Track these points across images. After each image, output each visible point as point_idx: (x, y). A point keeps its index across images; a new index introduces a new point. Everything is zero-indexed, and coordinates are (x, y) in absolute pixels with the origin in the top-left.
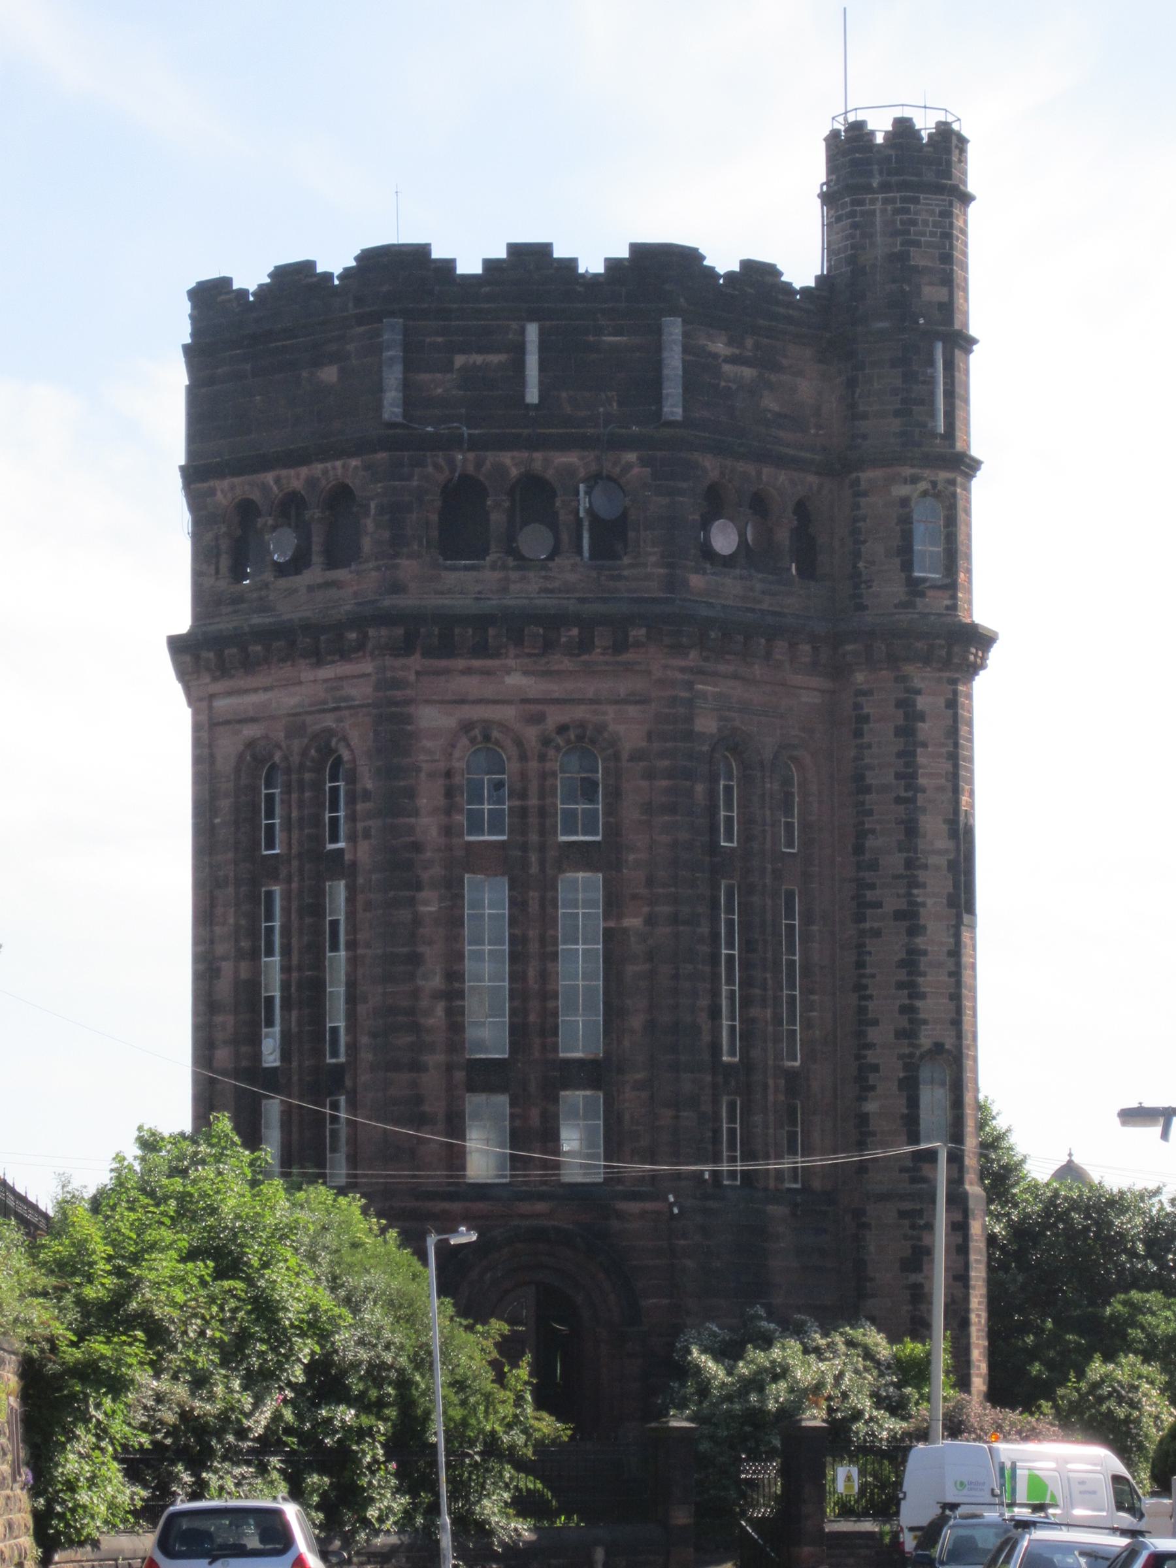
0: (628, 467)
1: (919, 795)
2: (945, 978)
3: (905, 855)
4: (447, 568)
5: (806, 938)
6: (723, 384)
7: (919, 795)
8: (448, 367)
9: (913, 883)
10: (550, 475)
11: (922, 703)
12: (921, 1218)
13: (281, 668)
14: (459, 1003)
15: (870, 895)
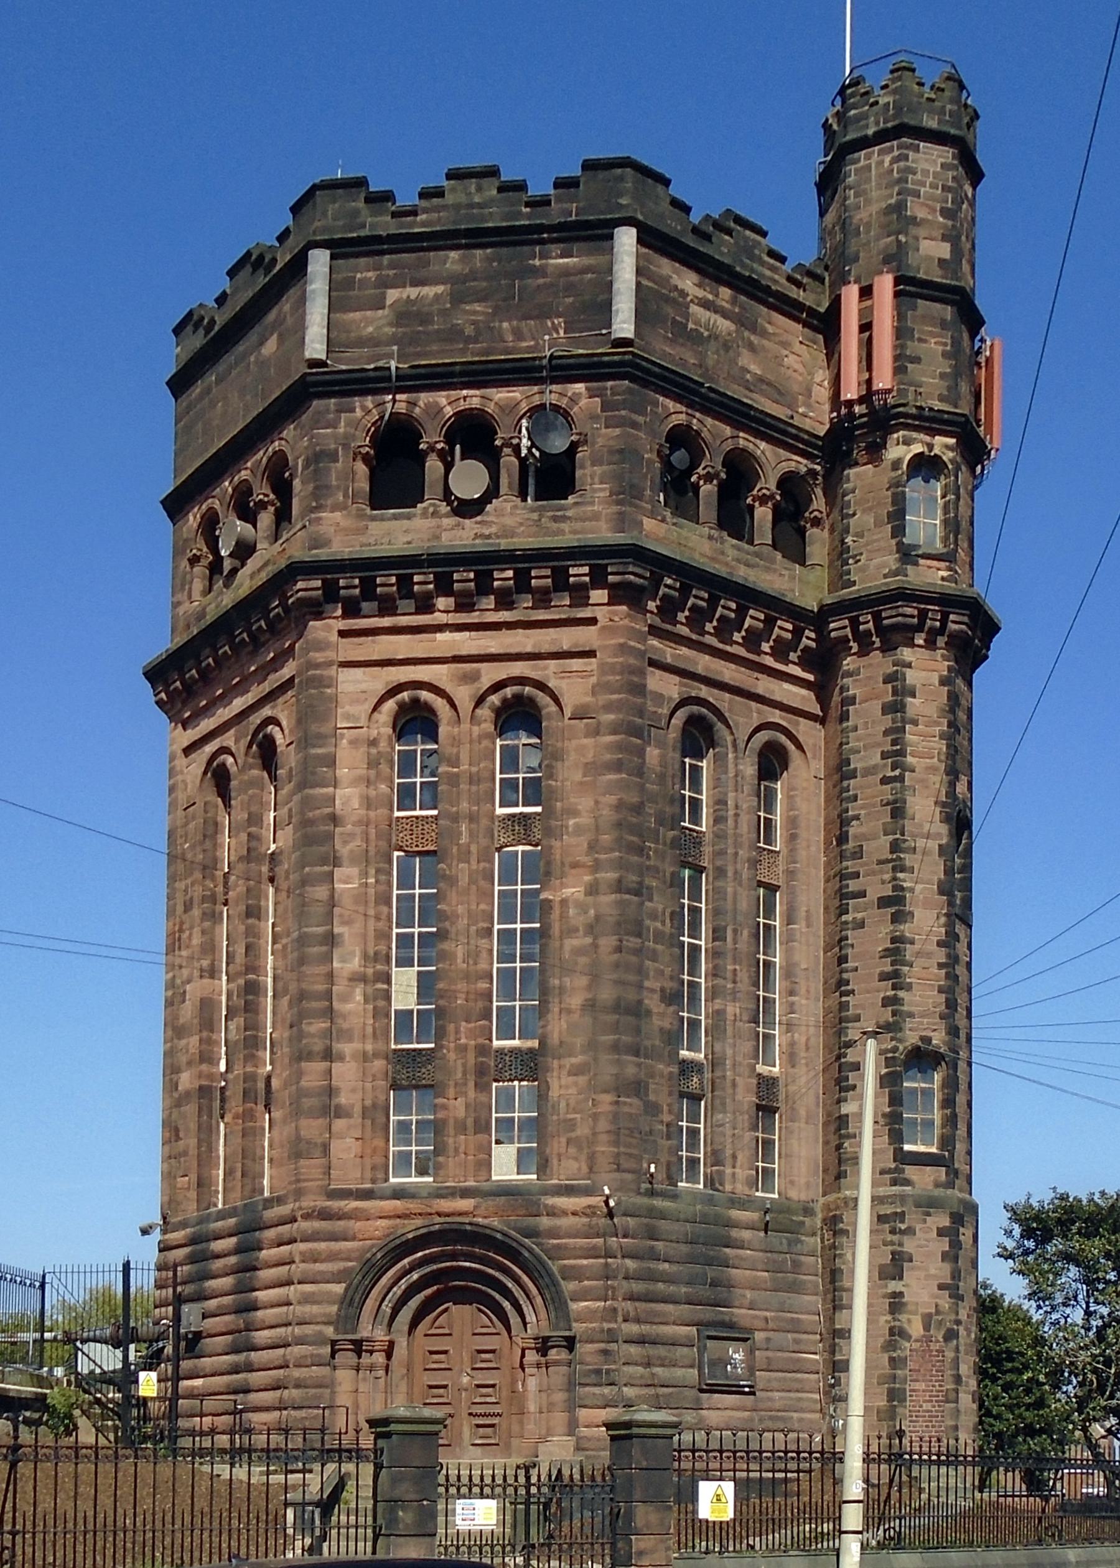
0: (574, 400)
1: (907, 774)
3: (891, 837)
4: (373, 519)
5: (789, 939)
6: (691, 326)
7: (907, 774)
8: (379, 304)
9: (899, 867)
10: (490, 409)
11: (912, 677)
15: (853, 885)
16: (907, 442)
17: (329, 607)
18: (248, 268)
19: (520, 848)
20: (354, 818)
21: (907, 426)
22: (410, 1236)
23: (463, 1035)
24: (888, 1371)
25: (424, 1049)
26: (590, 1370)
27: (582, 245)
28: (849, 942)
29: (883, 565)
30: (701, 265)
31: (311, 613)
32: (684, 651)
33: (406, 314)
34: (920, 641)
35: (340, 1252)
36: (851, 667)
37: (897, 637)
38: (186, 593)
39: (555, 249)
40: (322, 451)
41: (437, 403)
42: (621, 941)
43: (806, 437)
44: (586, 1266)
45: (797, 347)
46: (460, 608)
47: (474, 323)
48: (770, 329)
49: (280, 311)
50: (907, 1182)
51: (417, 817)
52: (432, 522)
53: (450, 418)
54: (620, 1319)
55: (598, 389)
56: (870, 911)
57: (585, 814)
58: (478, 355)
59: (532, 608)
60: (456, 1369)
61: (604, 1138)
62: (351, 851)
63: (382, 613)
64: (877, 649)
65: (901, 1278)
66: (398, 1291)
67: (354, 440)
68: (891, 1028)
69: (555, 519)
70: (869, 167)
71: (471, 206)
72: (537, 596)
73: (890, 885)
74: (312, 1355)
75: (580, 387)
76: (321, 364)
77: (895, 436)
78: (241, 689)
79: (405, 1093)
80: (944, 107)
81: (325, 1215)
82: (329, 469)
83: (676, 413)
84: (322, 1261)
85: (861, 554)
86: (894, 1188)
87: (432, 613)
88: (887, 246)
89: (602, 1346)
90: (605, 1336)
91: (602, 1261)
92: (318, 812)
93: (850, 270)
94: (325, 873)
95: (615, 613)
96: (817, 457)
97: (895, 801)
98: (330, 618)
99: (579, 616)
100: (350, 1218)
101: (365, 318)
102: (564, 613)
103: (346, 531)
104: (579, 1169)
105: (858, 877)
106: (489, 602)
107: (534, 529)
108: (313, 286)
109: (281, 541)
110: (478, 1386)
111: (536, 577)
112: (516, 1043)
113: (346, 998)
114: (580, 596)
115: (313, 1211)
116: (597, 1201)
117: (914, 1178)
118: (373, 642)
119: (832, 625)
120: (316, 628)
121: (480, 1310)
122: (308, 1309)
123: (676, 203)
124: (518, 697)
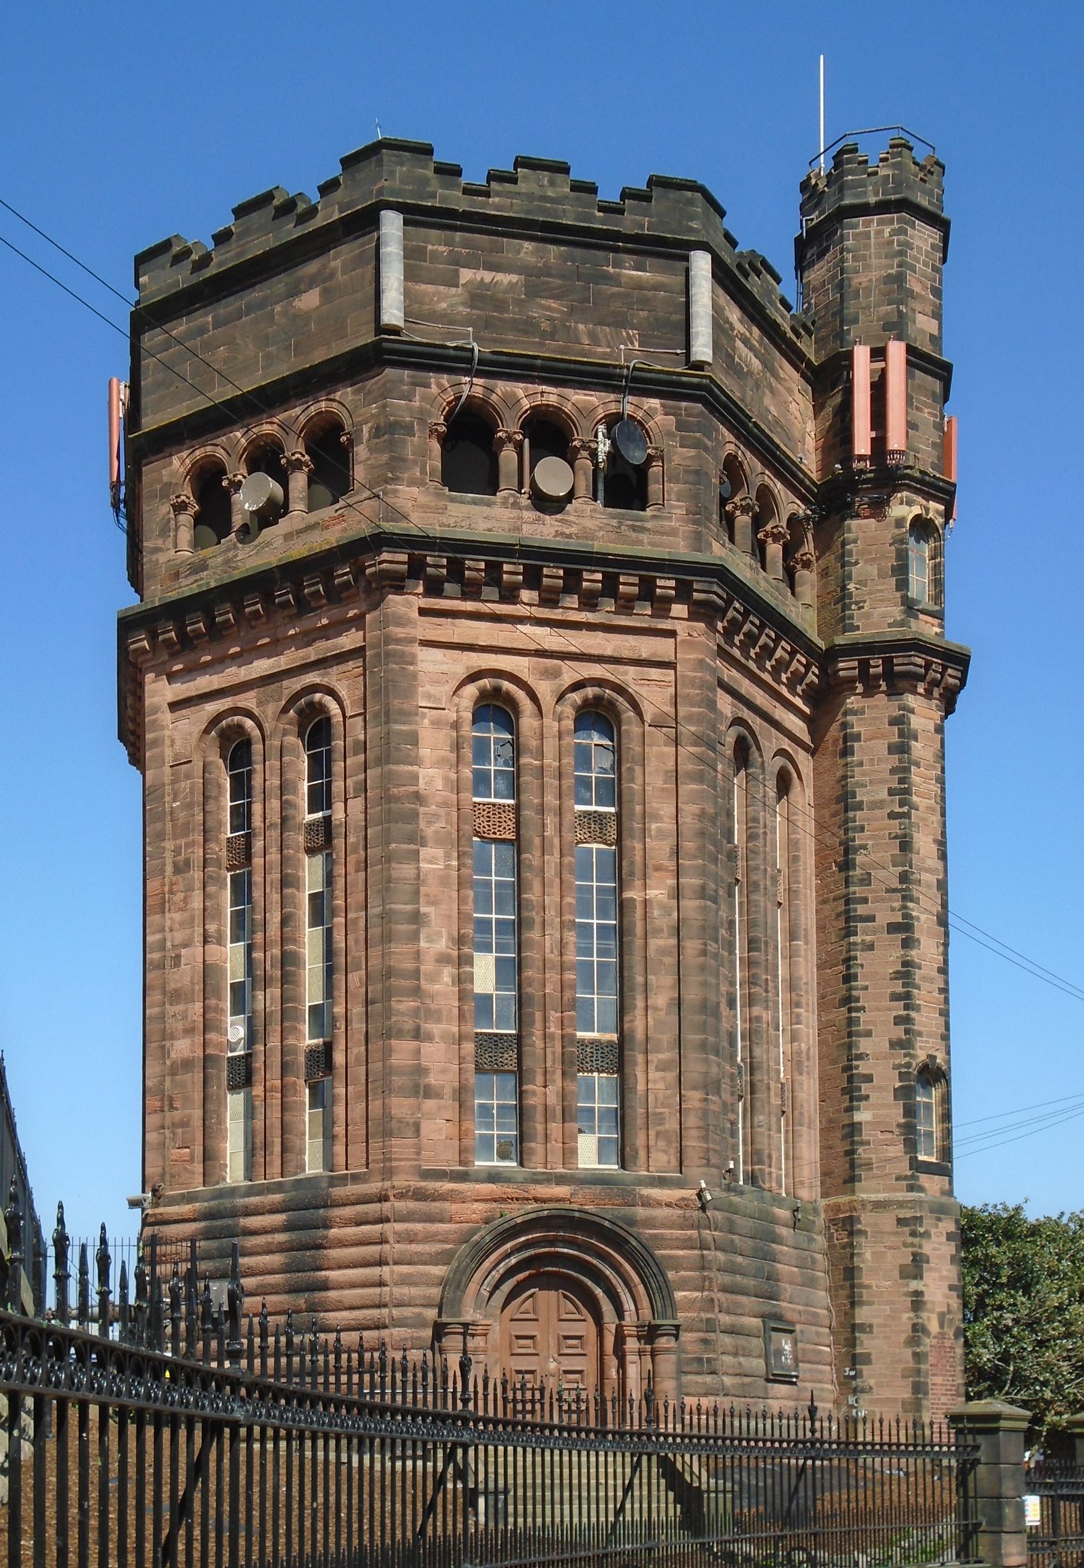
0: (649, 414)
2: (936, 994)
3: (900, 869)
4: (452, 500)
10: (568, 408)
11: (916, 722)
12: (921, 1226)
13: (253, 628)
14: (468, 969)
15: (861, 910)
16: (910, 503)
17: (409, 583)
18: (269, 211)
19: (595, 846)
20: (439, 799)
21: (909, 488)
22: (519, 1220)
23: (552, 1024)
24: (911, 1365)
25: (506, 1035)
26: (692, 1359)
27: (654, 260)
28: (859, 962)
29: (884, 616)
30: (746, 304)
31: (391, 587)
32: (734, 673)
33: (478, 296)
34: (921, 690)
35: (437, 1234)
36: (856, 706)
37: (903, 684)
38: (170, 539)
39: (628, 259)
40: (396, 423)
41: (514, 394)
42: (705, 944)
43: (808, 482)
44: (684, 1257)
45: (798, 396)
46: (544, 602)
47: (550, 319)
48: (782, 374)
49: (325, 266)
50: (921, 1189)
51: (494, 805)
52: (515, 513)
53: (526, 411)
54: (717, 1310)
55: (672, 408)
56: (879, 935)
57: (666, 820)
58: (554, 352)
59: (615, 613)
60: (543, 1354)
61: (694, 1133)
62: (436, 832)
63: (465, 597)
64: (882, 692)
65: (922, 1278)
66: (496, 1275)
67: (430, 417)
68: (903, 1044)
69: (634, 528)
70: (867, 235)
71: (545, 199)
72: (622, 602)
73: (900, 913)
74: (412, 1338)
75: (655, 403)
76: (395, 331)
77: (899, 495)
78: (274, 649)
79: (484, 1077)
80: (932, 190)
81: (420, 1195)
82: (404, 442)
83: (729, 443)
84: (418, 1242)
85: (865, 602)
86: (911, 1194)
87: (515, 604)
88: (888, 313)
89: (701, 1335)
90: (704, 1326)
91: (696, 1252)
92: (402, 789)
93: (849, 330)
94: (409, 851)
95: (694, 629)
96: (812, 503)
97: (905, 836)
98: (409, 594)
99: (660, 626)
100: (445, 1200)
101: (438, 293)
102: (646, 622)
103: (424, 508)
104: (669, 1162)
105: (867, 902)
106: (573, 601)
107: (613, 536)
108: (389, 249)
109: (337, 506)
110: (566, 1372)
111: (624, 584)
112: (594, 1035)
113: (434, 978)
114: (661, 608)
115: (408, 1191)
116: (691, 1194)
117: (926, 1185)
118: (453, 625)
119: (841, 665)
120: (396, 603)
121: (565, 1296)
122: (405, 1290)
123: (728, 236)
124: (598, 699)
